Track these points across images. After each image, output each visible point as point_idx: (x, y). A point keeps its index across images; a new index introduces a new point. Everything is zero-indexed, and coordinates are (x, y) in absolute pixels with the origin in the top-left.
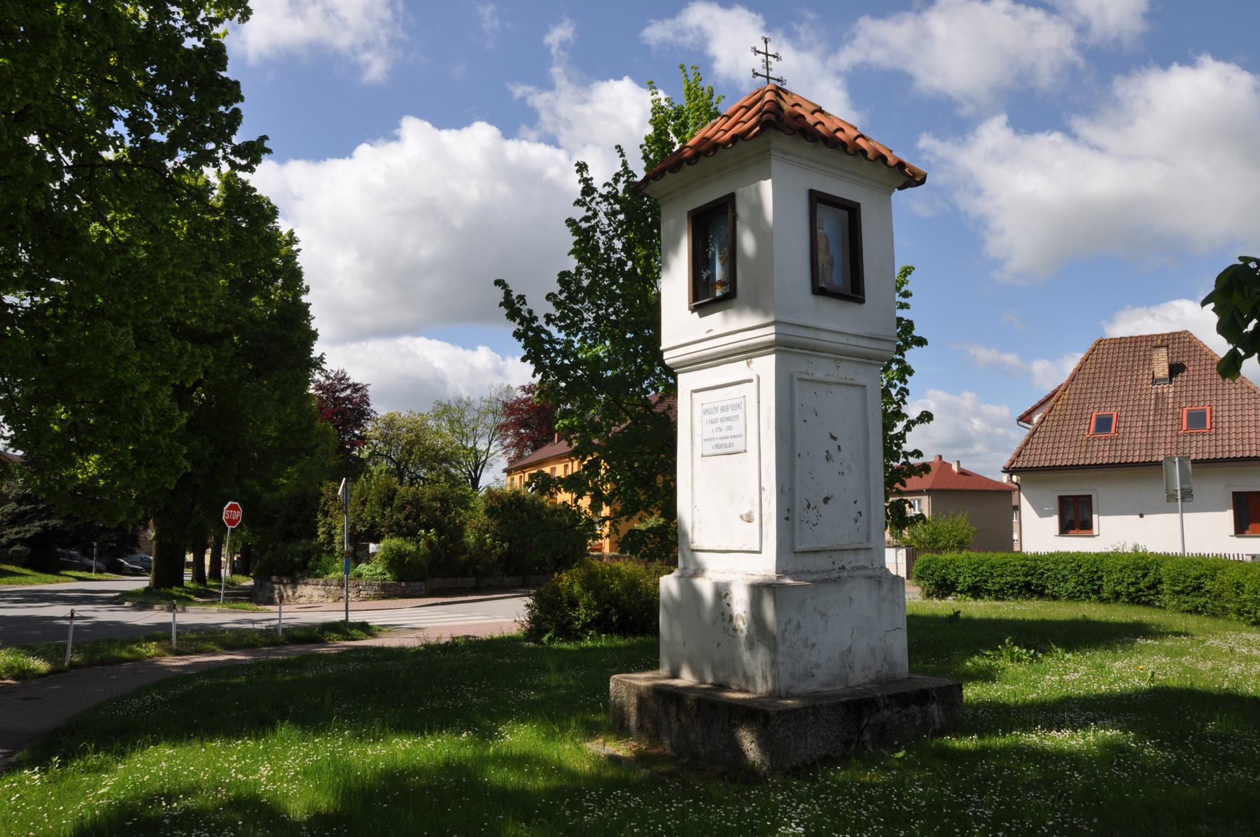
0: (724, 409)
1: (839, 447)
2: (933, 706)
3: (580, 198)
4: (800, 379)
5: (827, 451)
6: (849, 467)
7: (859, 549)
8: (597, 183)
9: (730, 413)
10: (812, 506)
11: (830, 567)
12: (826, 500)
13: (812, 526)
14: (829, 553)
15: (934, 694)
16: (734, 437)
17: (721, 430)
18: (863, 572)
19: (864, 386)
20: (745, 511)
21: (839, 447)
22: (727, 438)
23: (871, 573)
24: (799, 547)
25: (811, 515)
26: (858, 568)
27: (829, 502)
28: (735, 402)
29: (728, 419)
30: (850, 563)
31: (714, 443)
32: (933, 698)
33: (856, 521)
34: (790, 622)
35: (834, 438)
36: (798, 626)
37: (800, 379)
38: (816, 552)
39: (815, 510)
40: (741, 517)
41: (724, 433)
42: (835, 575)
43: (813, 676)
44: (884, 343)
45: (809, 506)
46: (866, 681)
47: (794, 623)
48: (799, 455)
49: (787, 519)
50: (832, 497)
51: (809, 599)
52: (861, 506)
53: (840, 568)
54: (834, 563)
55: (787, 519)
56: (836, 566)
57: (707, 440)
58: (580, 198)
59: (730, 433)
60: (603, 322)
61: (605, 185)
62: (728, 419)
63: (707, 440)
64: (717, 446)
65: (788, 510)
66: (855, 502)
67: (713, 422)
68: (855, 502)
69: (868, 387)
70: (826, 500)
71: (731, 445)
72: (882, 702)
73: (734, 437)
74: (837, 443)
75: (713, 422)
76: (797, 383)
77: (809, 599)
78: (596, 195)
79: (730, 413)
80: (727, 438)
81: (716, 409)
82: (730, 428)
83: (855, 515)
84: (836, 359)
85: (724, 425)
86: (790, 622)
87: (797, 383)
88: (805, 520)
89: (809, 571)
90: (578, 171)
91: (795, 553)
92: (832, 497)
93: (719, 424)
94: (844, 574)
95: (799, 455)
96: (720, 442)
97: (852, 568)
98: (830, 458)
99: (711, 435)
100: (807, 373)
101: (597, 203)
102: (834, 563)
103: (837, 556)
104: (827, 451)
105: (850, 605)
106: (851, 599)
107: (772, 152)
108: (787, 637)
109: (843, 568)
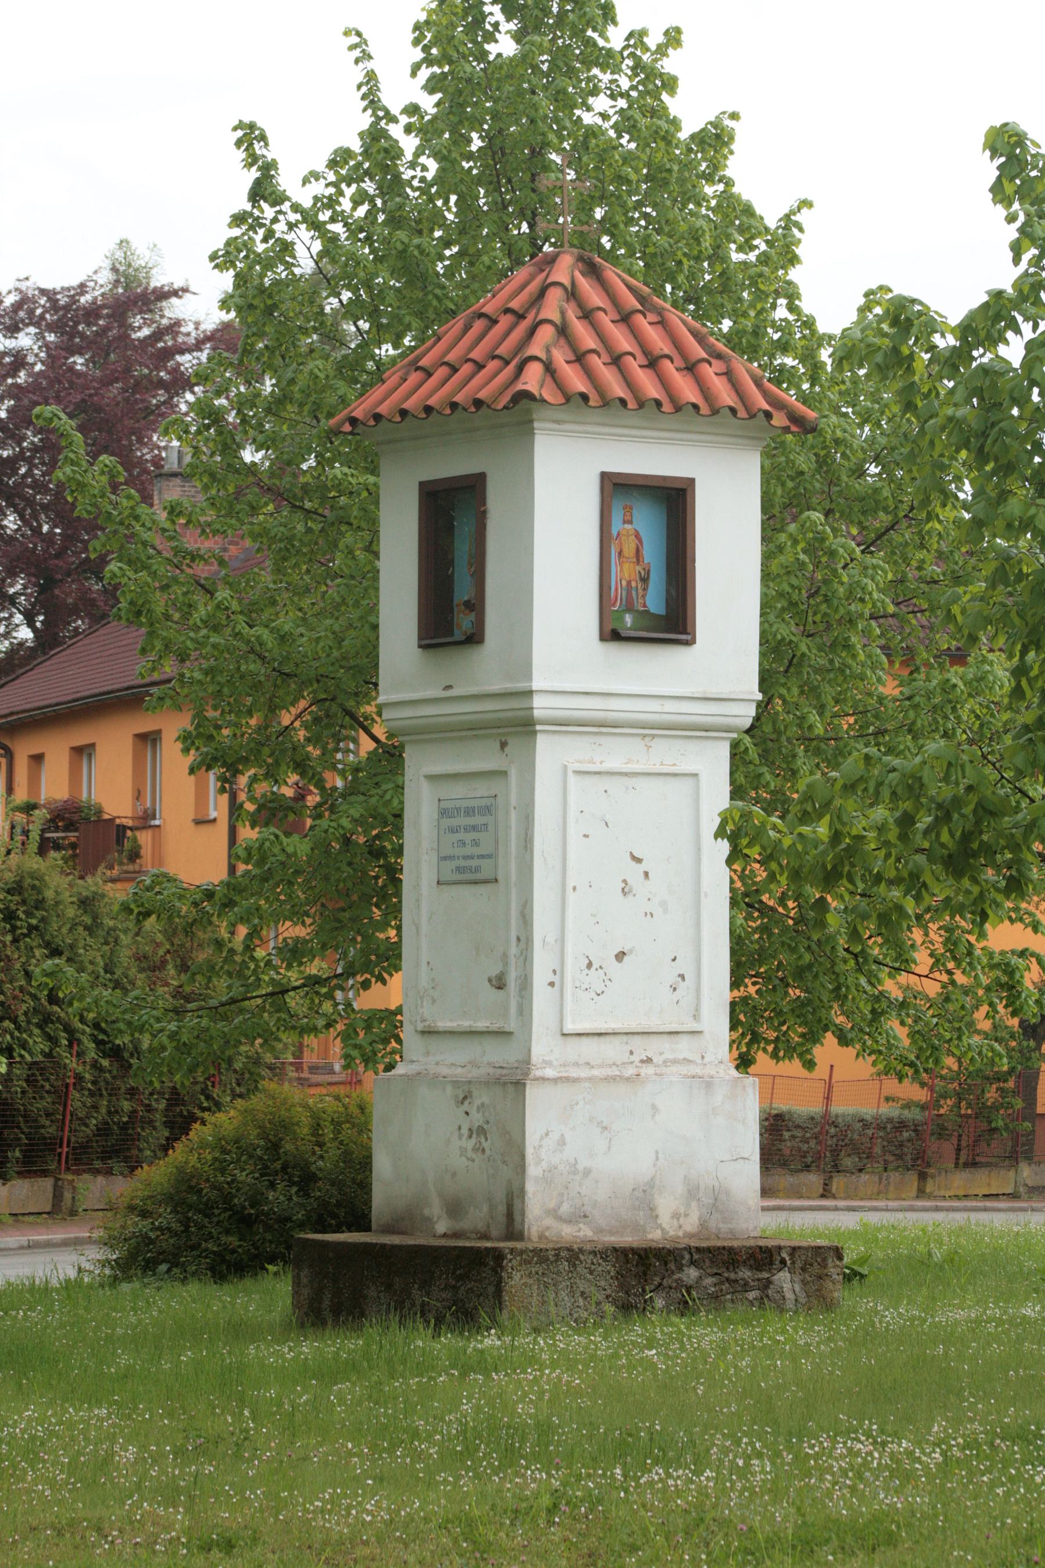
0: (469, 812)
1: (646, 874)
2: (781, 1274)
3: (248, 207)
4: (577, 773)
5: (625, 881)
6: (663, 904)
7: (677, 1033)
8: (288, 181)
9: (478, 820)
10: (595, 965)
11: (626, 1057)
12: (620, 956)
13: (594, 996)
14: (625, 1038)
15: (784, 1255)
16: (482, 857)
17: (464, 844)
18: (684, 1070)
19: (696, 775)
20: (494, 972)
21: (646, 874)
22: (472, 857)
23: (698, 1070)
24: (570, 1027)
25: (594, 978)
26: (675, 1062)
27: (626, 958)
28: (483, 802)
29: (474, 828)
30: (661, 1054)
31: (457, 863)
32: (783, 1262)
33: (675, 989)
34: (547, 1134)
35: (639, 861)
36: (562, 1142)
37: (577, 773)
38: (600, 1034)
39: (601, 972)
40: (490, 980)
41: (469, 850)
42: (630, 1071)
43: (585, 1216)
44: (731, 704)
45: (590, 965)
46: (681, 1234)
47: (555, 1136)
48: (574, 888)
49: (552, 984)
50: (631, 951)
51: (581, 1103)
52: (684, 965)
53: (642, 1061)
54: (631, 1053)
55: (552, 984)
56: (635, 1058)
57: (445, 858)
58: (248, 207)
59: (477, 851)
60: (131, 1497)
61: (305, 181)
62: (474, 828)
63: (445, 858)
64: (459, 870)
65: (554, 972)
66: (674, 960)
67: (453, 830)
68: (674, 960)
69: (703, 778)
70: (620, 956)
71: (478, 869)
72: (687, 1256)
73: (482, 857)
74: (643, 867)
75: (453, 830)
76: (572, 779)
77: (581, 1103)
78: (286, 206)
79: (478, 820)
80: (472, 857)
81: (458, 810)
82: (476, 843)
83: (672, 978)
84: (644, 736)
85: (468, 837)
86: (547, 1134)
87: (572, 779)
88: (584, 987)
89: (588, 1064)
90: (239, 143)
91: (564, 1035)
92: (631, 951)
93: (461, 836)
94: (648, 1070)
95: (574, 888)
96: (462, 863)
97: (665, 1062)
98: (630, 891)
99: (450, 852)
100: (592, 762)
101: (291, 226)
102: (631, 1053)
103: (637, 1042)
104: (625, 881)
105: (653, 1116)
106: (654, 1107)
107: (536, 425)
108: (543, 1156)
109: (649, 1060)
